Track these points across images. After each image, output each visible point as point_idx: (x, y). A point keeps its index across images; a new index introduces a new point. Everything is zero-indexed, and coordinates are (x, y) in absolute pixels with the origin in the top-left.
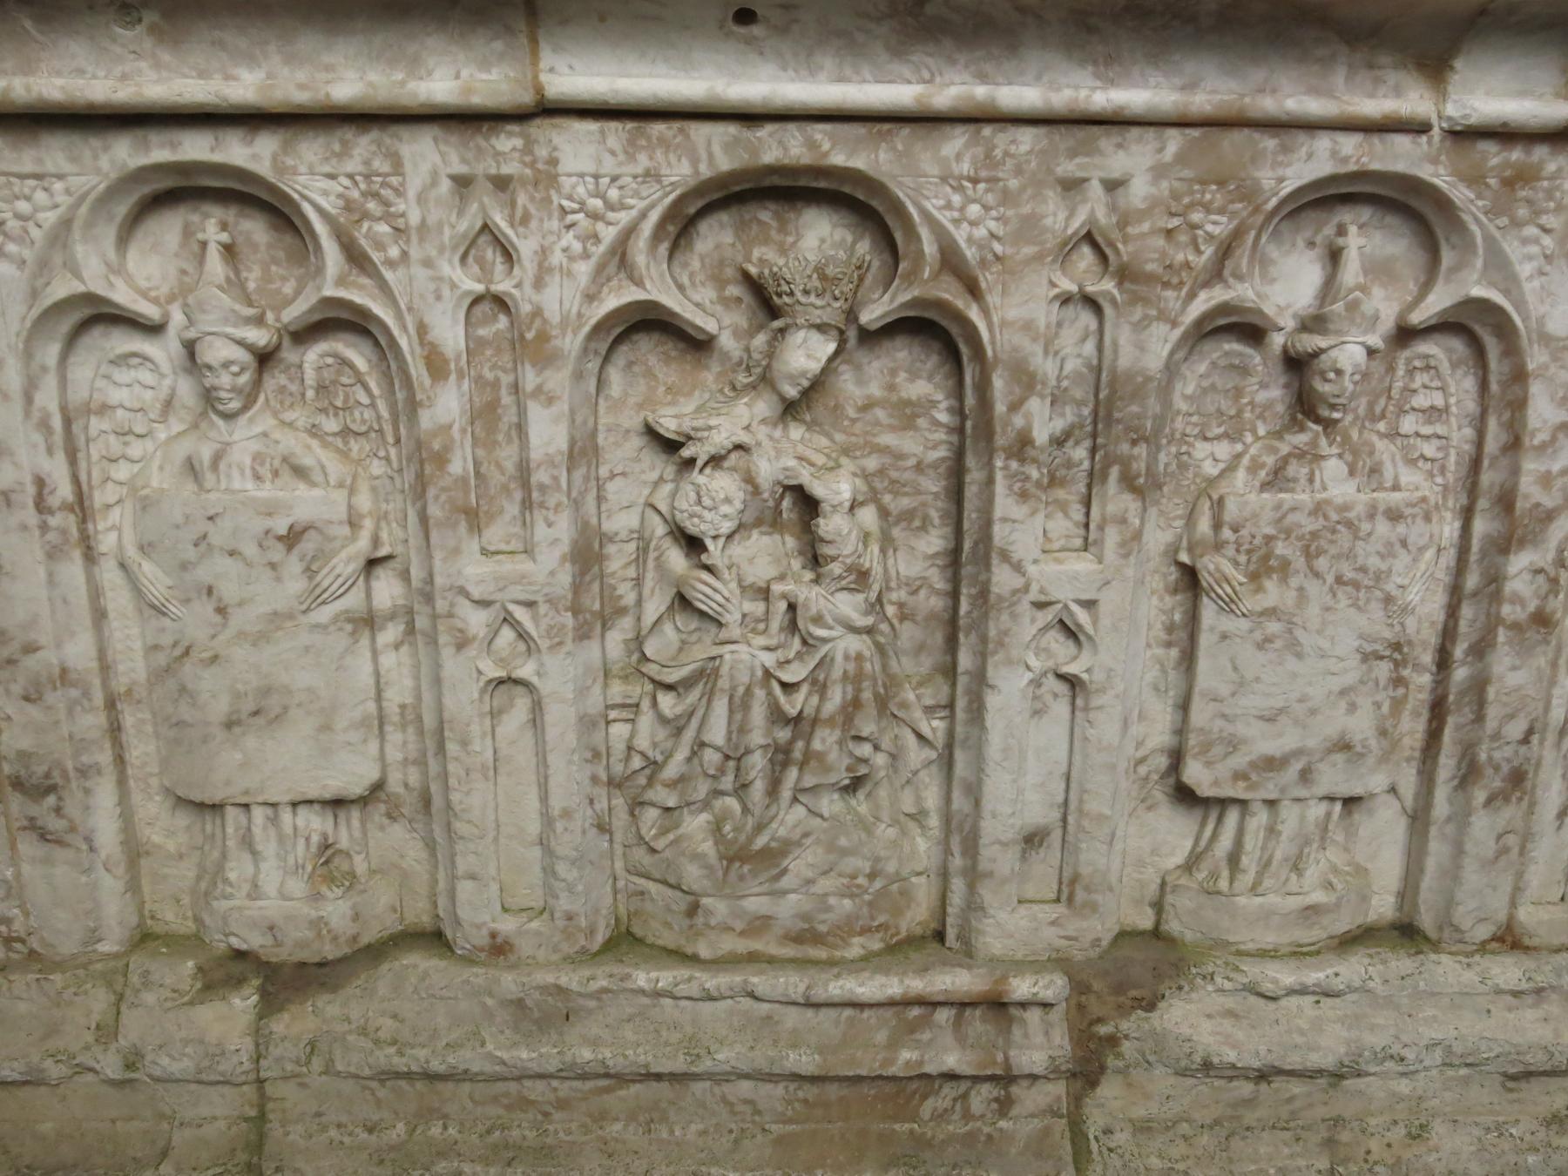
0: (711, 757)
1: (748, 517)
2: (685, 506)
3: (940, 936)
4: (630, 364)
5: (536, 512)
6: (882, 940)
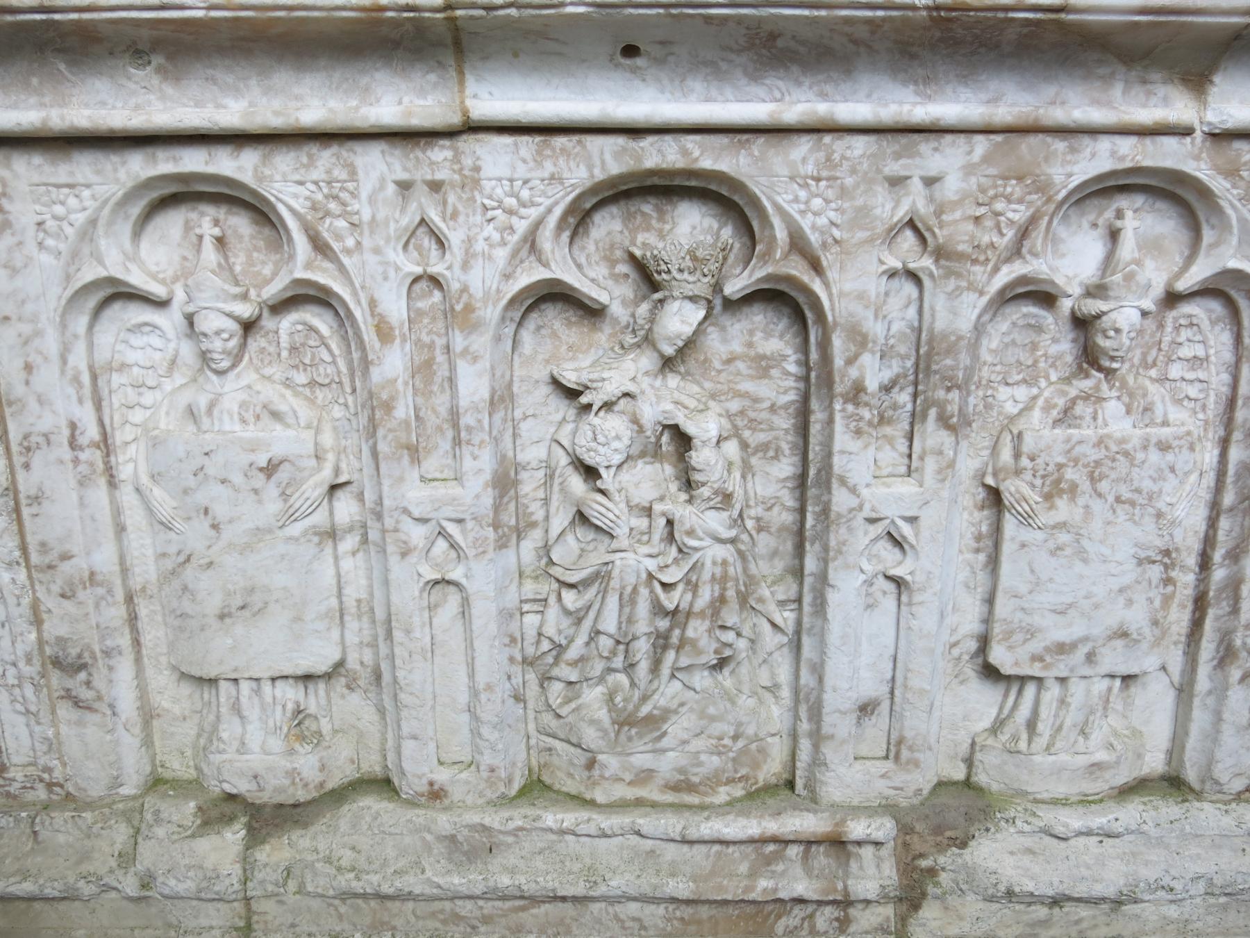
0: (605, 643)
1: (635, 450)
2: (583, 442)
3: (791, 785)
4: (539, 328)
5: (464, 447)
6: (744, 788)
